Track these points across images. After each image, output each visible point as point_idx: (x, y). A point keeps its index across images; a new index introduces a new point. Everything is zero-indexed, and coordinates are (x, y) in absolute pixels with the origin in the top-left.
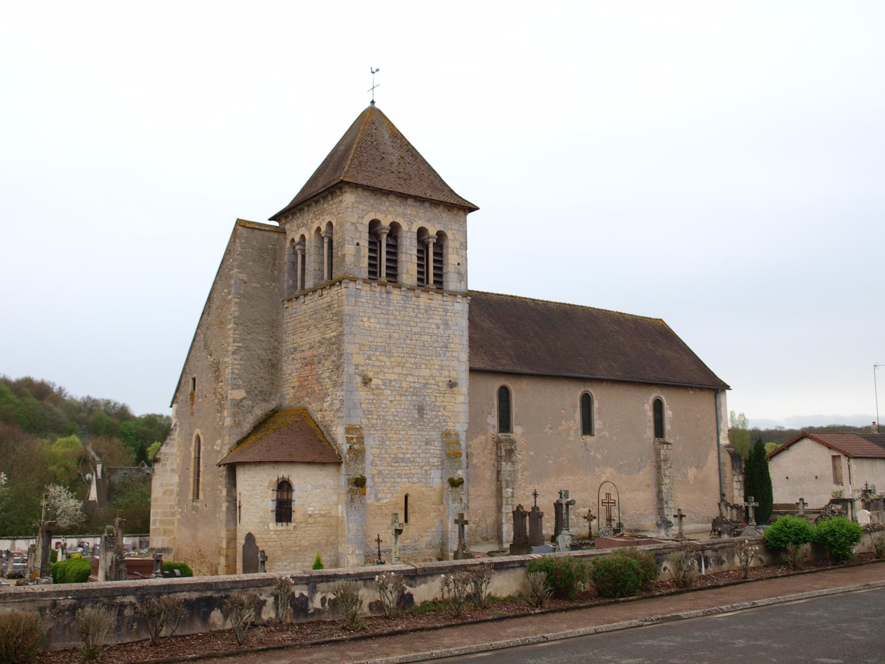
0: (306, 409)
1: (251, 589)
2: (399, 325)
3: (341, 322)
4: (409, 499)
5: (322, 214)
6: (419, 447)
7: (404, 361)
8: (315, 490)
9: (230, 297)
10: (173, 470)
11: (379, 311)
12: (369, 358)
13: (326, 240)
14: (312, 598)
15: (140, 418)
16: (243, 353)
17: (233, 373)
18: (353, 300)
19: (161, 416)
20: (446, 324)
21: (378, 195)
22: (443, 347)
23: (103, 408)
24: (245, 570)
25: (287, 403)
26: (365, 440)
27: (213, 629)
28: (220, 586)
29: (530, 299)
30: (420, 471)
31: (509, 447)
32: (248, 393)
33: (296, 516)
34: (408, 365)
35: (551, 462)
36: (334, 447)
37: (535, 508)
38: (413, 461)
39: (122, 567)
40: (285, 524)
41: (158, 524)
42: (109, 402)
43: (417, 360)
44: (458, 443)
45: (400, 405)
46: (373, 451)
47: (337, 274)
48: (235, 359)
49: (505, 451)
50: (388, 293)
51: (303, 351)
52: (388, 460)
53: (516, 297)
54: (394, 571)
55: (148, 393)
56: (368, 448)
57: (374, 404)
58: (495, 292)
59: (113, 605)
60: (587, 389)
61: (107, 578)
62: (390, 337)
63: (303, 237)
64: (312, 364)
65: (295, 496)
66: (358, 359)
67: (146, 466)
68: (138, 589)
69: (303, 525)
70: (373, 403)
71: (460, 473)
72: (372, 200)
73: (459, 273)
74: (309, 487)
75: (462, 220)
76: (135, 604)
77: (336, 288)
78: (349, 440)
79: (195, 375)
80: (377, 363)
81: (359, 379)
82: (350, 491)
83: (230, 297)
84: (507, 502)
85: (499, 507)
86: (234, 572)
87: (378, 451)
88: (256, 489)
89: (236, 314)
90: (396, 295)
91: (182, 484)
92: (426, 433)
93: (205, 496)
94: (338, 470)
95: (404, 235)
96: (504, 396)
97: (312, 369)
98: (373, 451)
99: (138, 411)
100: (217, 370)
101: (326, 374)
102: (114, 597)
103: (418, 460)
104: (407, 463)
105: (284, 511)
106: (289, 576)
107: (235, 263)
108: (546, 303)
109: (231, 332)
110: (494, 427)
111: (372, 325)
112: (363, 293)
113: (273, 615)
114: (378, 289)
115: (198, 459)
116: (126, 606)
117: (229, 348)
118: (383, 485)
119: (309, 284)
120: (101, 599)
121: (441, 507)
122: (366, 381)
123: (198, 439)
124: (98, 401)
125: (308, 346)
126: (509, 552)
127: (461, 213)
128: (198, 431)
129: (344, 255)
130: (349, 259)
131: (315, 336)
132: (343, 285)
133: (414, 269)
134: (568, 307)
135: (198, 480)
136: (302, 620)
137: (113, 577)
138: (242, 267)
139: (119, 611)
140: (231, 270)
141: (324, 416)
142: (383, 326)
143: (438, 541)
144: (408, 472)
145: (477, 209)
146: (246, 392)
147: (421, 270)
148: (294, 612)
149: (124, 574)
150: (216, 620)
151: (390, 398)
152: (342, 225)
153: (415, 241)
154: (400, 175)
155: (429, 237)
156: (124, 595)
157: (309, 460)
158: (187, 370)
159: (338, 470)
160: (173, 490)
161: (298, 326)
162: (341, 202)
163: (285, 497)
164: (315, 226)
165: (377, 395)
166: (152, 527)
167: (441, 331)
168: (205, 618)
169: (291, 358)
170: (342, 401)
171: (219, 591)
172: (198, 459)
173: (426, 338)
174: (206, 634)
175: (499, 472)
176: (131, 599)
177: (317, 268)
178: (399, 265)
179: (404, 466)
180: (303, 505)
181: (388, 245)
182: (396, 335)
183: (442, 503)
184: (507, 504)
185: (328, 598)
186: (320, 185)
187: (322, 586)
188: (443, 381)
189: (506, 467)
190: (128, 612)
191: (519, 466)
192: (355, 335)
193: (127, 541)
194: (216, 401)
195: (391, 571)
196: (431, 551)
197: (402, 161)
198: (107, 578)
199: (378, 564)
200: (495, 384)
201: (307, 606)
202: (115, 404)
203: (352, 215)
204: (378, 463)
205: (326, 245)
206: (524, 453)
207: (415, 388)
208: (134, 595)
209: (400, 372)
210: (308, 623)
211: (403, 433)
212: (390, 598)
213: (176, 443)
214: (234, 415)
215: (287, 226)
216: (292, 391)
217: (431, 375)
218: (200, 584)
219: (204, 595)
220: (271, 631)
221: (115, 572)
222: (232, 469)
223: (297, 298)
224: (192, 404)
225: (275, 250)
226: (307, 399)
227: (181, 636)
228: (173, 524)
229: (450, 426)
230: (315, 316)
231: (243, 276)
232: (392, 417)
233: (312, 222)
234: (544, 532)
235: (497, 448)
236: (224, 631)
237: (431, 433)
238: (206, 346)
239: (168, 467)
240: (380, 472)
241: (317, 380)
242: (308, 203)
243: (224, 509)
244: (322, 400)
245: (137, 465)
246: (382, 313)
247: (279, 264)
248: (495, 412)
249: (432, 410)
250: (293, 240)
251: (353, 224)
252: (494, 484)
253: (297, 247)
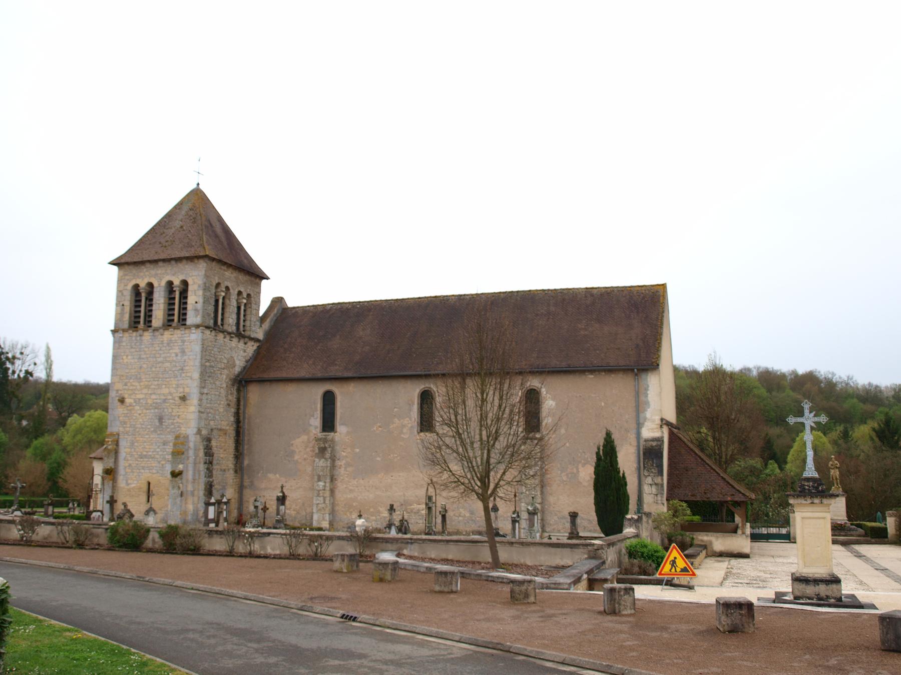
11: (133, 350)
20: (183, 352)
31: (322, 445)
35: (378, 459)
90: (147, 336)
98: (127, 450)
108: (460, 297)
151: (139, 412)
167: (179, 358)
182: (145, 366)
229: (183, 430)
248: (318, 414)
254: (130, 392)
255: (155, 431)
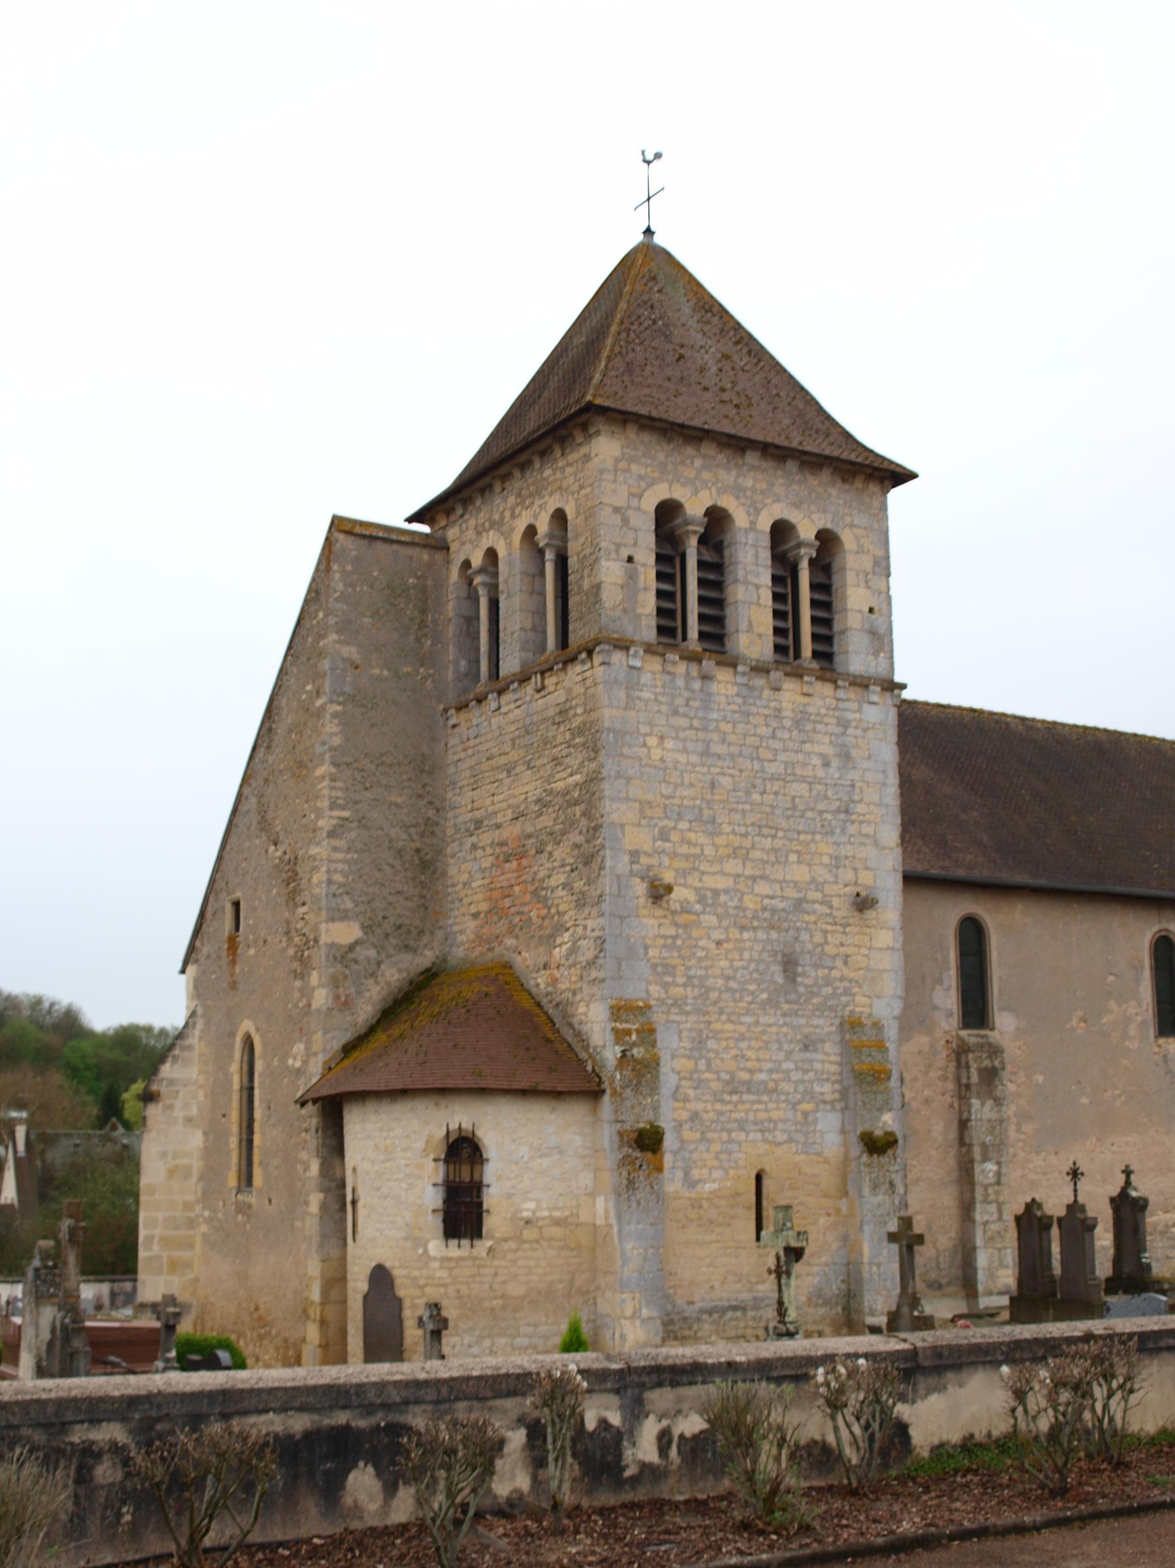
0: (508, 966)
1: (461, 1405)
2: (733, 757)
3: (594, 749)
4: (767, 1183)
5: (538, 493)
6: (788, 1055)
7: (747, 843)
8: (537, 1157)
9: (319, 703)
10: (189, 1120)
11: (682, 722)
12: (664, 836)
13: (549, 556)
14: (631, 1433)
15: (103, 1035)
16: (353, 835)
17: (330, 882)
18: (622, 694)
19: (149, 1029)
20: (845, 756)
21: (666, 463)
22: (838, 811)
23: (26, 1013)
24: (372, 1354)
25: (459, 953)
26: (658, 1036)
27: (356, 1525)
28: (371, 1394)
29: (1014, 717)
30: (790, 1115)
31: (986, 1063)
32: (367, 929)
33: (494, 1223)
34: (757, 854)
35: (1085, 1100)
36: (583, 1055)
37: (1075, 1208)
38: (774, 1090)
39: (78, 1343)
40: (465, 1242)
41: (156, 1247)
42: (38, 1001)
43: (778, 843)
44: (881, 1046)
45: (741, 951)
46: (679, 1064)
47: (578, 634)
48: (335, 849)
49: (976, 1072)
50: (706, 677)
51: (498, 826)
52: (715, 1085)
53: (981, 712)
54: (866, 1356)
55: (126, 975)
56: (665, 1058)
57: (679, 949)
58: (933, 699)
59: (60, 1452)
60: (1164, 925)
61: (41, 1372)
62: (713, 785)
63: (491, 554)
64: (520, 856)
65: (491, 1173)
66: (638, 838)
67: (121, 1130)
68: (133, 1402)
69: (511, 1245)
70: (673, 947)
71: (888, 1121)
72: (661, 452)
73: (873, 633)
74: (524, 1151)
75: (876, 503)
76: (124, 1448)
77: (578, 668)
78: (620, 1036)
79: (238, 894)
80: (684, 850)
81: (640, 888)
82: (625, 1161)
83: (319, 703)
84: (986, 1195)
85: (967, 1209)
86: (343, 1359)
87: (690, 1065)
88: (392, 1156)
89: (336, 741)
90: (725, 684)
91: (212, 1150)
92: (803, 1021)
93: (267, 1177)
94: (594, 1111)
95: (741, 538)
96: (972, 939)
97: (520, 869)
98: (679, 1064)
99: (101, 1018)
100: (294, 877)
101: (559, 878)
102: (64, 1427)
103: (785, 1087)
104: (758, 1093)
105: (462, 1213)
106: (573, 1367)
107: (332, 620)
108: (1052, 727)
109: (326, 783)
110: (949, 1015)
111: (670, 757)
112: (646, 678)
113: (523, 1482)
114: (681, 668)
115: (249, 1091)
116: (98, 1456)
117: (321, 823)
118: (702, 1147)
119: (510, 664)
120: (25, 1432)
121: (843, 1205)
122: (659, 893)
123: (249, 1044)
124: (16, 997)
125: (509, 814)
126: (1006, 1315)
127: (874, 488)
128: (247, 1026)
129: (598, 587)
130: (611, 596)
131: (529, 787)
132: (597, 659)
133: (765, 621)
134: (1104, 737)
135: (250, 1142)
136: (607, 1498)
137: (56, 1369)
138: (346, 629)
139: (80, 1469)
140: (321, 637)
141: (555, 981)
142: (694, 759)
143: (835, 1287)
144: (762, 1115)
145: (912, 476)
146: (363, 927)
147: (780, 624)
148: (585, 1473)
149: (82, 1363)
150: (363, 1498)
151: (717, 935)
152: (589, 514)
153: (766, 555)
154: (726, 396)
155: (799, 545)
156: (94, 1421)
157: (523, 1085)
158: (220, 884)
159: (594, 1111)
160: (189, 1167)
161: (485, 766)
162: (587, 458)
163: (466, 1177)
164: (521, 526)
165: (685, 926)
166: (142, 1254)
167: (834, 772)
168: (331, 1491)
169: (468, 845)
170: (601, 942)
171: (369, 1409)
172: (249, 1091)
173: (800, 789)
174: (335, 1542)
175: (963, 1124)
176: (112, 1432)
177: (528, 624)
178: (729, 611)
179: (754, 1104)
180: (510, 1196)
181: (702, 565)
182: (726, 781)
183: (846, 1194)
184: (985, 1201)
185: (676, 1433)
186: (531, 424)
187: (660, 1398)
188: (840, 896)
189: (981, 1110)
190: (106, 1472)
191: (1010, 1110)
192: (629, 780)
193: (88, 1292)
194: (291, 952)
195: (857, 1356)
196: (822, 1311)
197: (727, 366)
198: (41, 1372)
199: (780, 1335)
200: (950, 912)
201: (619, 1456)
202: (52, 1004)
203: (615, 489)
204: (691, 1092)
205: (549, 569)
206: (1021, 1078)
207: (774, 911)
208: (124, 1420)
209: (739, 870)
210: (624, 1506)
211: (748, 1019)
212: (846, 1436)
213: (195, 1055)
214: (335, 982)
215: (452, 533)
216: (472, 924)
217: (813, 880)
218: (313, 1390)
219: (327, 1422)
220: (528, 1533)
221: (60, 1358)
222: (332, 1110)
223: (479, 701)
224: (233, 963)
225: (424, 590)
226: (510, 942)
227: (262, 1547)
228: (191, 1246)
230: (526, 741)
231: (350, 652)
232: (720, 982)
233: (513, 516)
234: (1098, 1273)
235: (958, 1066)
236: (387, 1532)
237: (816, 1022)
238: (264, 824)
239: (179, 1113)
240: (695, 1116)
241: (535, 893)
242: (503, 470)
243: (314, 1208)
244: (550, 940)
245: (101, 1128)
246: (691, 727)
247: (435, 621)
249: (816, 966)
250: (467, 564)
251: (616, 510)
252: (953, 1152)
253: (478, 580)
254: (680, 864)
255: (772, 1003)
